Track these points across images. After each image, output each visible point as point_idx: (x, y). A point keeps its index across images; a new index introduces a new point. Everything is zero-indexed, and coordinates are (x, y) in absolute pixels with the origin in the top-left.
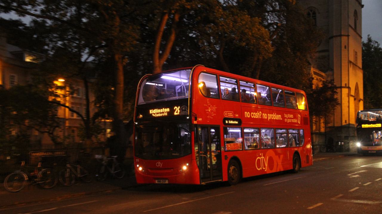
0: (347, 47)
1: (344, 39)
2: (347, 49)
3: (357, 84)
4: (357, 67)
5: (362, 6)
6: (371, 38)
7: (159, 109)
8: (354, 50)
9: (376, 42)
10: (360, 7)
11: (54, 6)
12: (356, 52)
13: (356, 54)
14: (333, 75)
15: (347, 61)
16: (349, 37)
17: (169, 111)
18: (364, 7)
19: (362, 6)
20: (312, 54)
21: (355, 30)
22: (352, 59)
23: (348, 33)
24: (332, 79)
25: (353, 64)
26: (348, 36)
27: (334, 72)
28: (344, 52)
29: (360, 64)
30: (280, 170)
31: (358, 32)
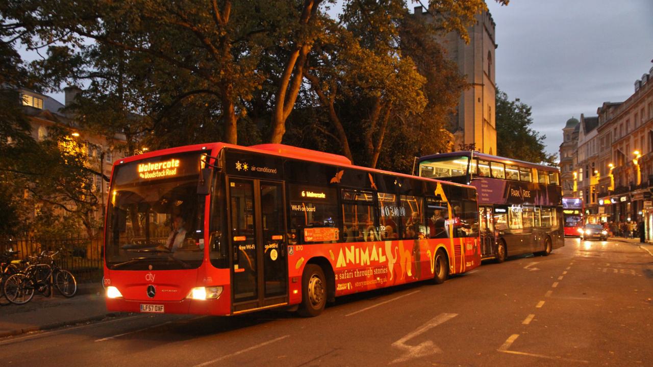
0: (481, 100)
1: (478, 89)
2: (481, 103)
3: (491, 149)
4: (491, 127)
5: (496, 46)
6: (499, 89)
7: (314, 192)
8: (488, 105)
9: (505, 94)
10: (494, 47)
11: (86, 29)
12: (490, 107)
13: (490, 110)
14: (464, 136)
15: (481, 119)
16: (484, 87)
17: (140, 165)
18: (498, 47)
19: (496, 46)
20: (106, 111)
21: (489, 77)
22: (486, 117)
23: (483, 82)
24: (472, 143)
25: (487, 122)
26: (483, 85)
27: (464, 133)
28: (478, 106)
29: (493, 123)
30: (374, 259)
31: (491, 79)
